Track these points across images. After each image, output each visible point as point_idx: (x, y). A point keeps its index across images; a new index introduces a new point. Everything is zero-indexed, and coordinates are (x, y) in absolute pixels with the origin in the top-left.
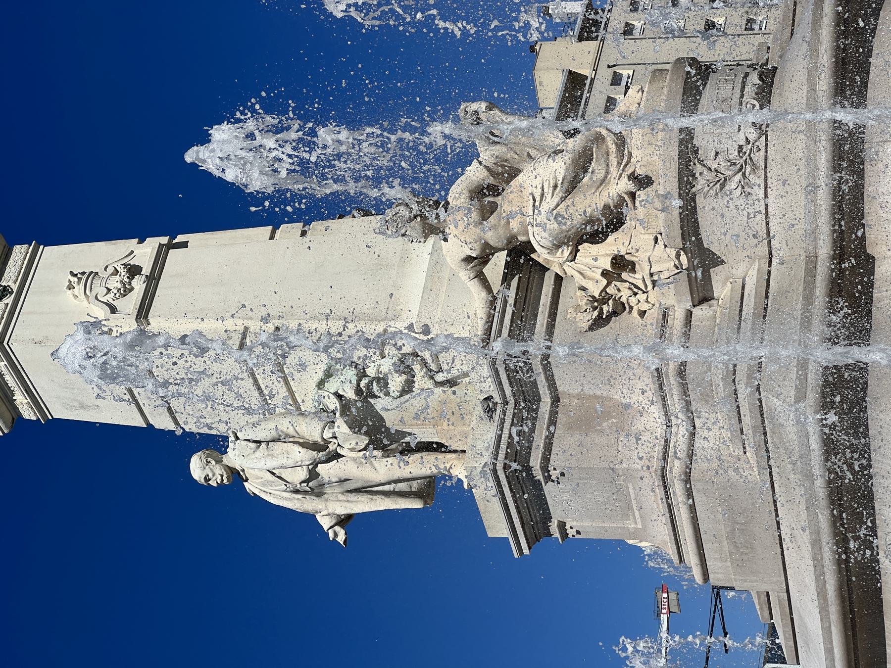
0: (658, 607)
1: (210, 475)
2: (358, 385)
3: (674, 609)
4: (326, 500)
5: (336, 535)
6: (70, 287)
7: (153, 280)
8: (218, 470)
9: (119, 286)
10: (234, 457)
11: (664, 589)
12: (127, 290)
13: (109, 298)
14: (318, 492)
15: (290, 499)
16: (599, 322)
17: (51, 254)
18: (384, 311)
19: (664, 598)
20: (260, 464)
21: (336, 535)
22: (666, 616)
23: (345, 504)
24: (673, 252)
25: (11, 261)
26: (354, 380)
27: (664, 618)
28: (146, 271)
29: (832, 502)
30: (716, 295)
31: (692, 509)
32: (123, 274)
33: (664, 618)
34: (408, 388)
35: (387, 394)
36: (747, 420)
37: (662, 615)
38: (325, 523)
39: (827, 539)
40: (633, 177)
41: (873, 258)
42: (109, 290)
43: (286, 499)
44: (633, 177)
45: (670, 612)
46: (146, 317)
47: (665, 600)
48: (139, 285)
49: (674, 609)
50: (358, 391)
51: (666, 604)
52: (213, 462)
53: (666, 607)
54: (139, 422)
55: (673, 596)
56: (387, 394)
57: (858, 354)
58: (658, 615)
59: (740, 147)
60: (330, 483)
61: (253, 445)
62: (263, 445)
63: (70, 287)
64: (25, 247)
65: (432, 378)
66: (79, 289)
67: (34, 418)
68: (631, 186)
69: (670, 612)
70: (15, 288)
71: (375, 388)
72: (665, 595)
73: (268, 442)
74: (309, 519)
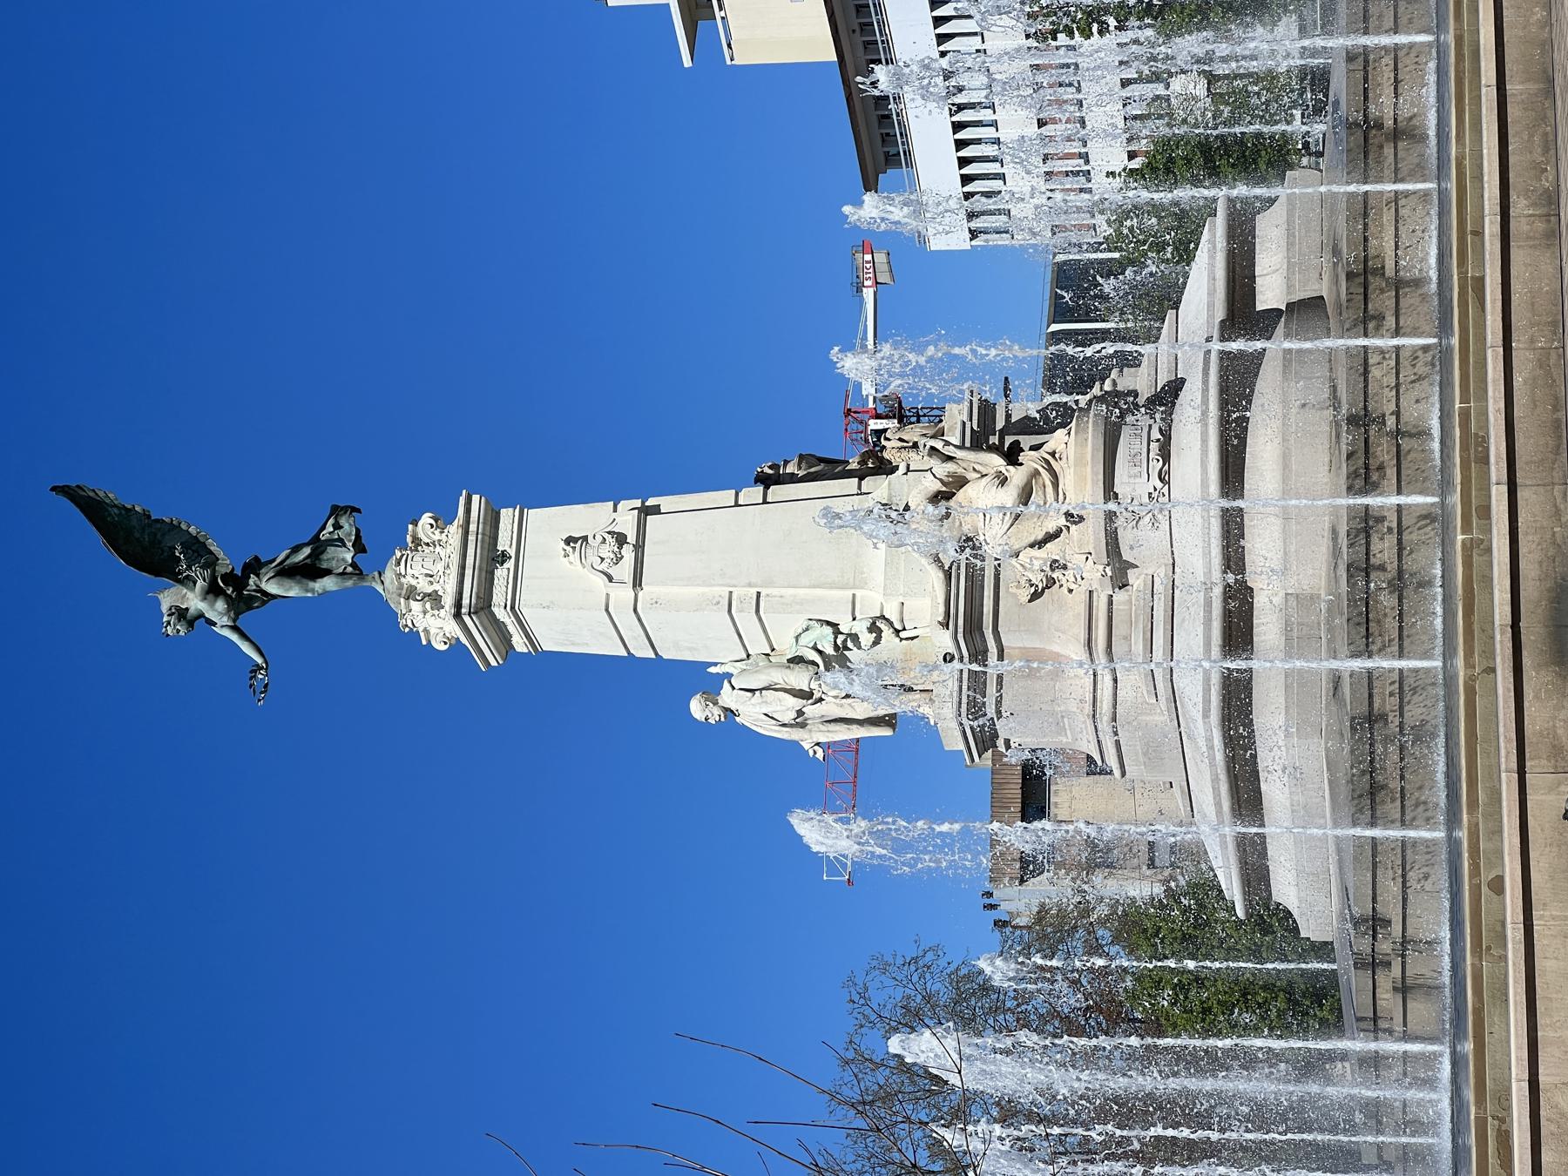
0: (858, 277)
1: (710, 716)
2: (835, 642)
3: (884, 277)
4: (810, 731)
5: (815, 752)
6: (566, 555)
7: (639, 547)
8: (717, 711)
9: (612, 556)
10: (727, 697)
11: (867, 248)
12: (619, 559)
13: (604, 567)
14: (803, 725)
15: (779, 731)
16: (1035, 596)
17: (534, 515)
18: (852, 580)
19: (868, 262)
20: (757, 709)
21: (815, 752)
22: (871, 291)
23: (827, 734)
24: (1101, 567)
25: (501, 525)
26: (831, 638)
27: (868, 294)
28: (631, 538)
29: (1226, 746)
30: (1131, 582)
31: (1118, 744)
32: (612, 544)
33: (868, 294)
34: (876, 642)
35: (859, 648)
36: (1160, 686)
37: (864, 290)
38: (806, 746)
39: (1223, 777)
40: (1068, 515)
41: (1252, 589)
42: (603, 559)
43: (775, 731)
44: (1068, 515)
45: (877, 283)
46: (640, 585)
47: (868, 266)
48: (628, 553)
49: (884, 277)
50: (836, 647)
51: (871, 270)
52: (711, 705)
53: (871, 275)
54: (623, 653)
55: (881, 258)
56: (859, 648)
57: (1237, 503)
58: (859, 289)
59: (1150, 494)
60: (814, 718)
61: (749, 694)
62: (757, 693)
63: (566, 555)
64: (511, 510)
65: (898, 636)
66: (574, 557)
67: (526, 651)
68: (1062, 521)
69: (877, 283)
70: (512, 553)
71: (850, 644)
72: (868, 257)
73: (761, 690)
74: (796, 745)
